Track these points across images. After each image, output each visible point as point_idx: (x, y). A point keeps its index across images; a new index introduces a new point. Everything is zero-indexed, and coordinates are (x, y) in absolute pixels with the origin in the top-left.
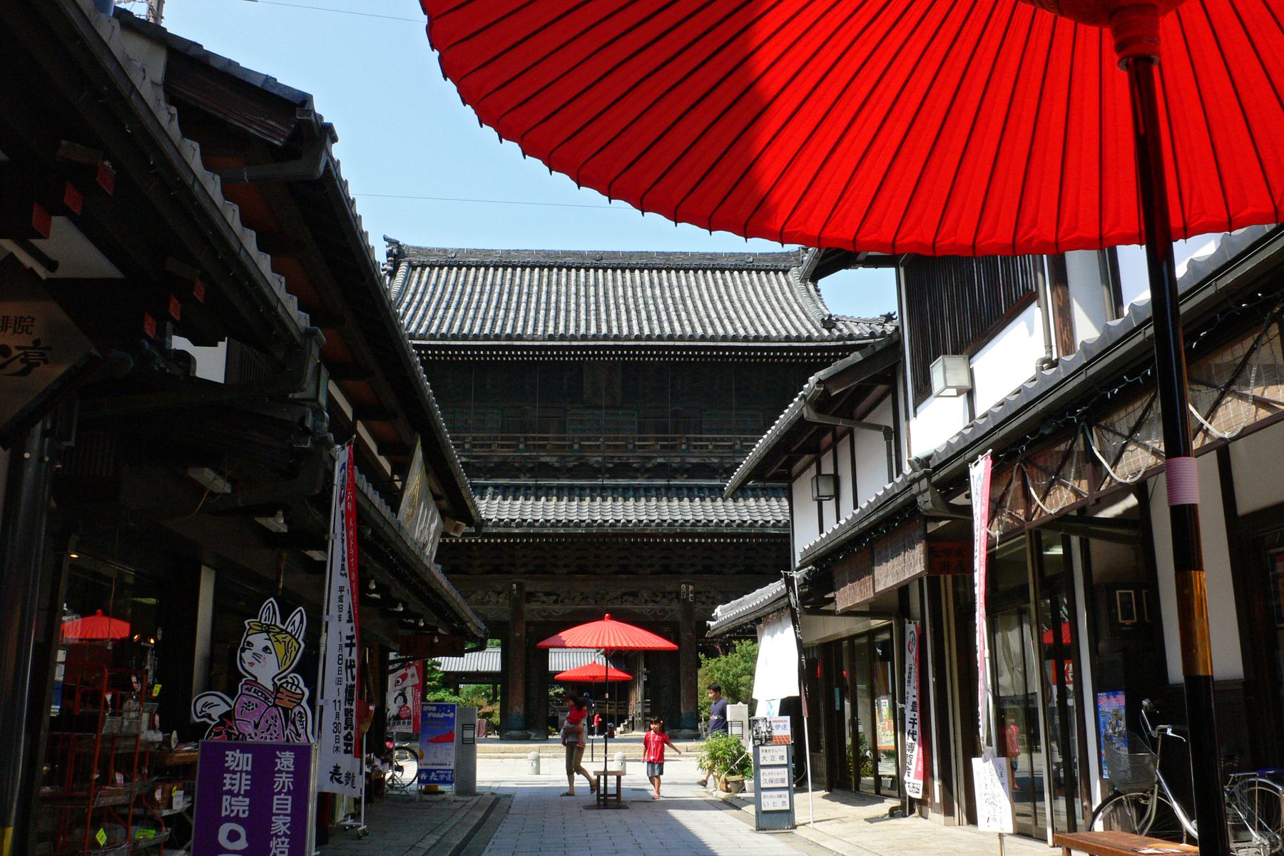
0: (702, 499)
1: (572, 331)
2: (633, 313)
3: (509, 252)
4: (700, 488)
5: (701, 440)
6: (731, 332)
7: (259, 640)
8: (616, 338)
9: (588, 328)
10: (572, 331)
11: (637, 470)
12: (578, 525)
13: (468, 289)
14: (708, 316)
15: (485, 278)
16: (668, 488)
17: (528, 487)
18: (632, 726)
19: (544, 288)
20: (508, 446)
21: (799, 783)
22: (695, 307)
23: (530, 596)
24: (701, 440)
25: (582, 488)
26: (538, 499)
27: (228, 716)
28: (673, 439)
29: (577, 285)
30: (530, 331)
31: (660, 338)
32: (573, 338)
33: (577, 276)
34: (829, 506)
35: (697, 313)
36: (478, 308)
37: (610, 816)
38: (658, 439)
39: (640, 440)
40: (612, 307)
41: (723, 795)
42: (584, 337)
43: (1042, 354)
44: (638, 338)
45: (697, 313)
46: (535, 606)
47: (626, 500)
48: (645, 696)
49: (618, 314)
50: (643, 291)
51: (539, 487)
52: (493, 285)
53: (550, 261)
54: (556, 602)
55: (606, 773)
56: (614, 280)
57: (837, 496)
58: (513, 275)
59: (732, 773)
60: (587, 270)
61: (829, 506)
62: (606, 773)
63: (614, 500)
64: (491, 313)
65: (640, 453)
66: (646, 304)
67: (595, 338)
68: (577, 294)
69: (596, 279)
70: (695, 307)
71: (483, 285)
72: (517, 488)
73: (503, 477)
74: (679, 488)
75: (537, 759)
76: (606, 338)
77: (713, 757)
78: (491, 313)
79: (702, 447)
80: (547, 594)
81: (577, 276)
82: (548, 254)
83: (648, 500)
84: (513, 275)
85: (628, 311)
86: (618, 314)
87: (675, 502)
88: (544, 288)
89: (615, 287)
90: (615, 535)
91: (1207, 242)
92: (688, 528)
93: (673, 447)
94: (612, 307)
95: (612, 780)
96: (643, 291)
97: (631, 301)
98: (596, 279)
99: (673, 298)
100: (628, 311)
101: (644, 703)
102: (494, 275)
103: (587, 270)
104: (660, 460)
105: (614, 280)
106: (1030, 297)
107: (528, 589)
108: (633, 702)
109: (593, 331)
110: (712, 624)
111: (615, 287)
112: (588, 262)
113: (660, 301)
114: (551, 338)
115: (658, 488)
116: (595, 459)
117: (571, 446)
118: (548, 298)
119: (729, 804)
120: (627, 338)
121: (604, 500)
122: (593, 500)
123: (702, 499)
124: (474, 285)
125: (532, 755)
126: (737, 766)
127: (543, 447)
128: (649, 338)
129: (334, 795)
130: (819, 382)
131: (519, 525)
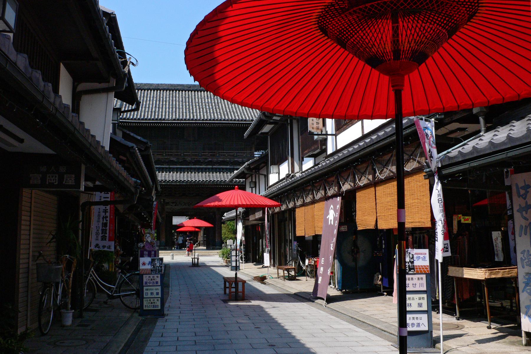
0: (223, 173)
1: (181, 117)
2: (201, 109)
3: (158, 84)
4: (223, 169)
5: (224, 153)
6: (234, 118)
7: (148, 235)
8: (196, 120)
9: (186, 116)
10: (181, 117)
11: (202, 163)
12: (183, 182)
13: (145, 99)
14: (226, 111)
15: (150, 94)
16: (212, 168)
17: (166, 168)
18: (199, 245)
19: (171, 99)
20: (161, 155)
21: (434, 306)
22: (222, 106)
23: (167, 204)
24: (224, 153)
25: (184, 168)
26: (170, 172)
27: (144, 246)
28: (214, 152)
29: (182, 97)
30: (167, 117)
31: (210, 120)
32: (182, 120)
33: (182, 93)
34: (254, 189)
35: (223, 109)
36: (149, 107)
37: (196, 268)
38: (209, 153)
39: (203, 152)
40: (194, 107)
41: (225, 264)
42: (185, 120)
43: (287, 173)
44: (203, 120)
45: (223, 109)
46: (168, 207)
47: (199, 173)
48: (204, 234)
49: (196, 110)
50: (205, 100)
51: (170, 168)
52: (153, 97)
53: (173, 88)
54: (175, 205)
55: (195, 258)
56: (195, 95)
57: (255, 187)
58: (160, 93)
59: (228, 258)
60: (185, 91)
61: (254, 189)
62: (195, 258)
63: (195, 173)
64: (154, 110)
65: (204, 157)
66: (205, 105)
67: (189, 120)
68: (182, 101)
69: (189, 95)
70: (222, 106)
71: (150, 97)
72: (163, 168)
73: (159, 165)
74: (216, 168)
75: (173, 255)
76: (192, 120)
77: (223, 254)
78: (154, 110)
79: (224, 155)
80: (173, 203)
81: (182, 93)
82: (172, 85)
83: (206, 173)
84: (160, 93)
85: (199, 109)
86: (196, 110)
87: (215, 174)
88: (171, 99)
89: (195, 98)
90: (195, 185)
91: (310, 160)
92: (218, 183)
93: (214, 155)
94: (194, 107)
95: (196, 260)
96: (205, 100)
97: (200, 104)
98: (189, 95)
99: (215, 103)
100: (199, 109)
101: (203, 236)
102: (154, 93)
103: (185, 91)
104: (210, 159)
105: (195, 95)
106: (286, 159)
107: (167, 201)
108: (199, 236)
109: (188, 117)
110: (224, 218)
111: (195, 98)
112: (186, 88)
113: (210, 104)
114: (174, 120)
115: (209, 168)
116: (188, 159)
117: (180, 155)
118: (172, 103)
119: (226, 266)
120: (199, 120)
121: (191, 173)
122: (188, 173)
123: (223, 173)
124: (147, 97)
125: (171, 254)
126: (227, 256)
127: (172, 155)
128: (206, 120)
129: (321, 235)
130: (248, 165)
131: (164, 182)
